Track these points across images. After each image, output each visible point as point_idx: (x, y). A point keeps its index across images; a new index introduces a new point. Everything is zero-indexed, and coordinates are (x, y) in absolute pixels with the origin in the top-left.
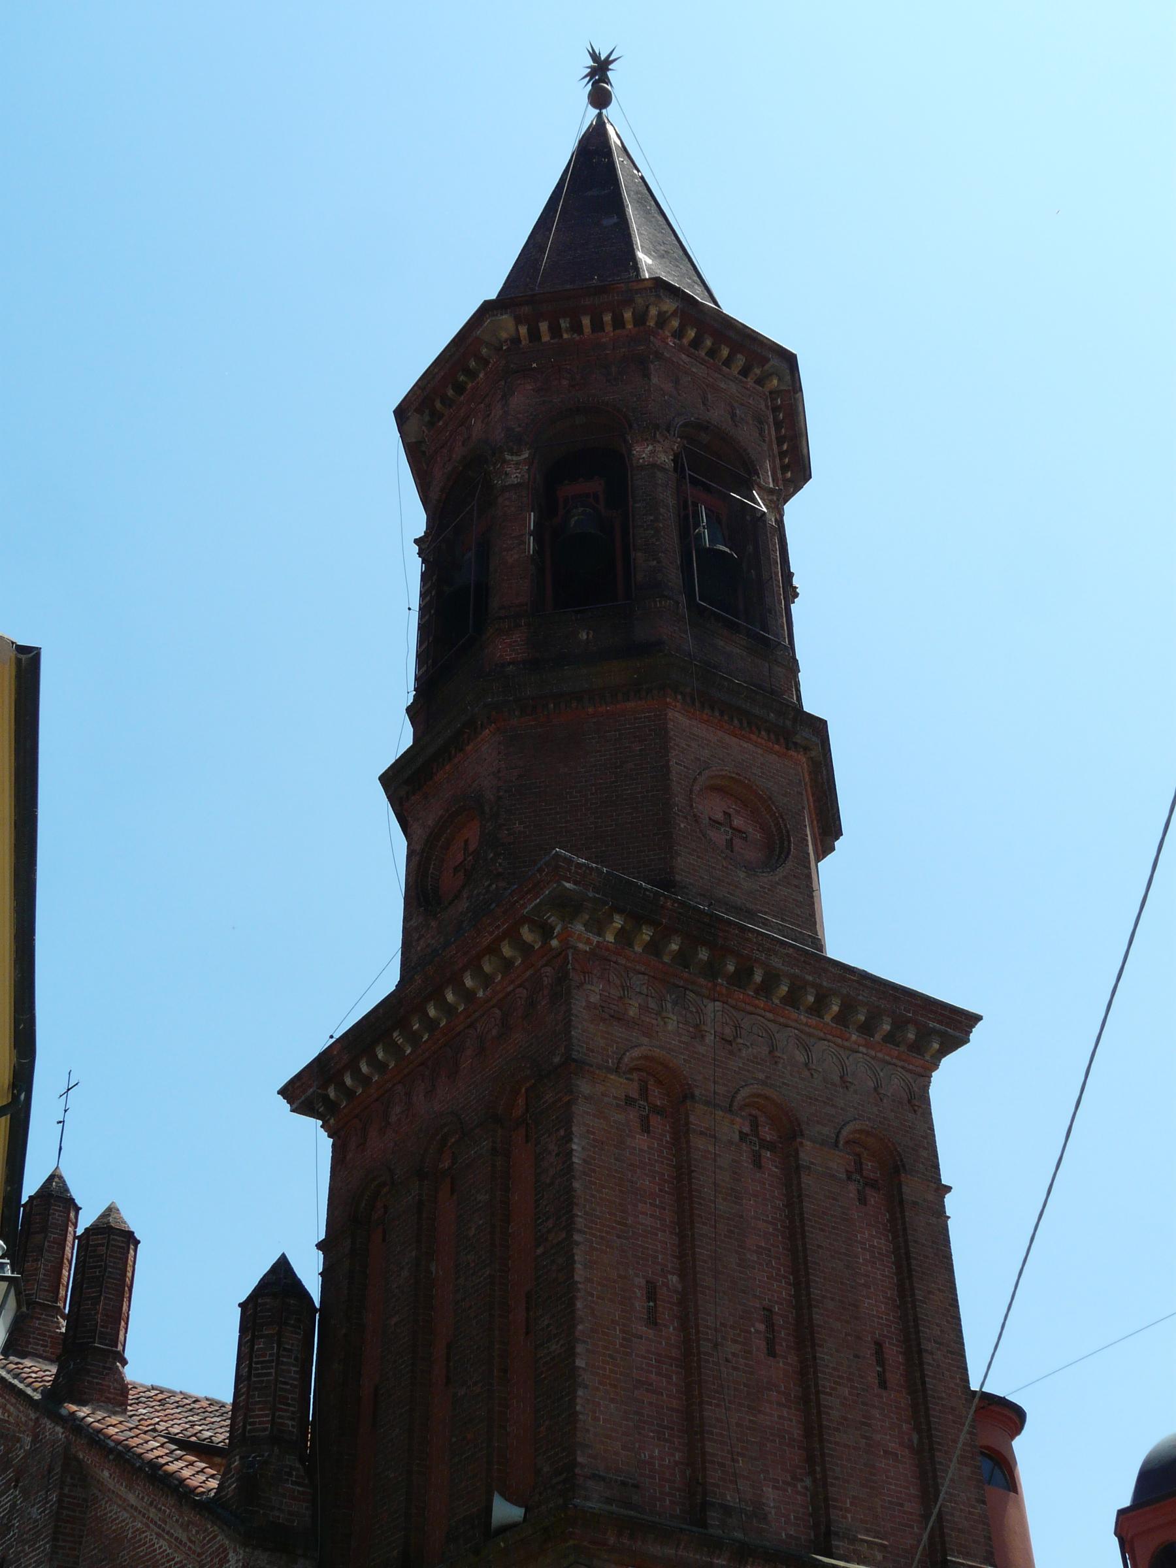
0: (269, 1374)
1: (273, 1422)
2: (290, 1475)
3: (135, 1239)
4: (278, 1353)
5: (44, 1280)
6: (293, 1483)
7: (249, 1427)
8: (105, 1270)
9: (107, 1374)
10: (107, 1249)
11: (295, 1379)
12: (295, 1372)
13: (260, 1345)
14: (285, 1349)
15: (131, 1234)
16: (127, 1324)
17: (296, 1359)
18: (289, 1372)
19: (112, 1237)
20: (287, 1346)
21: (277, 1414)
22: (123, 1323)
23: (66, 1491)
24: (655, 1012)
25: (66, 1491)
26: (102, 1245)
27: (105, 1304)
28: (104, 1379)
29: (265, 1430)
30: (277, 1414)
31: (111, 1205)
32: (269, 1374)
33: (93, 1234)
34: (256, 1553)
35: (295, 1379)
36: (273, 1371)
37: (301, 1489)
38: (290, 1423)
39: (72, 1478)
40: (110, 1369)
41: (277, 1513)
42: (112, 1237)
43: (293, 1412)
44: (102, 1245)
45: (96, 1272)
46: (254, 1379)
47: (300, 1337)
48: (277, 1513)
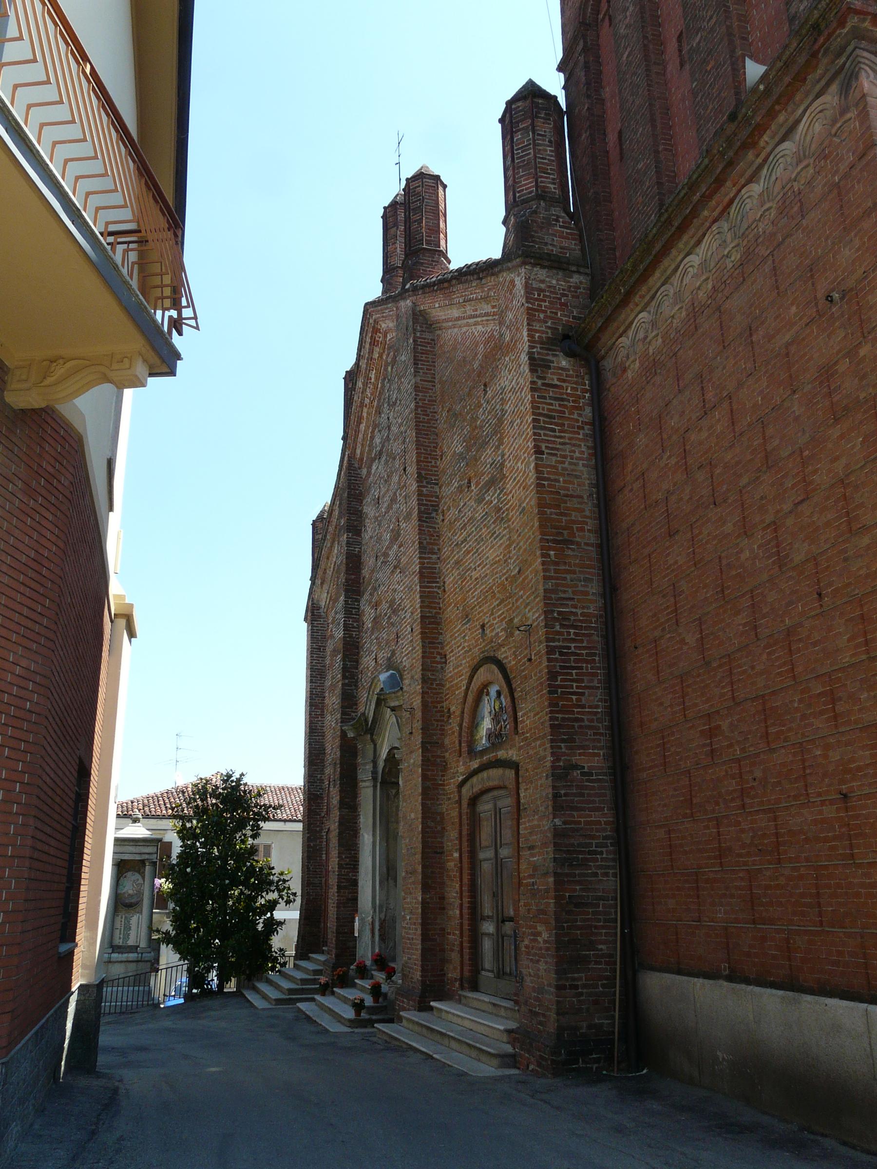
0: (529, 154)
1: (537, 186)
2: (557, 220)
3: (442, 183)
4: (533, 137)
5: (401, 254)
6: (560, 226)
7: (518, 195)
8: (423, 201)
9: (435, 265)
10: (423, 187)
11: (552, 156)
12: (551, 151)
13: (518, 136)
14: (539, 135)
15: (437, 178)
16: (446, 237)
17: (550, 141)
18: (546, 151)
19: (424, 180)
20: (540, 133)
21: (540, 180)
22: (442, 236)
23: (418, 334)
24: (801, 60)
25: (418, 334)
26: (419, 186)
27: (426, 222)
28: (434, 268)
29: (532, 192)
30: (540, 180)
31: (421, 169)
32: (529, 154)
33: (412, 182)
34: (535, 269)
35: (552, 156)
36: (531, 151)
37: (569, 231)
38: (552, 186)
39: (420, 327)
40: (438, 262)
41: (550, 247)
42: (424, 180)
43: (553, 179)
44: (419, 186)
45: (577, 687)
46: (516, 161)
47: (551, 126)
48: (550, 247)
